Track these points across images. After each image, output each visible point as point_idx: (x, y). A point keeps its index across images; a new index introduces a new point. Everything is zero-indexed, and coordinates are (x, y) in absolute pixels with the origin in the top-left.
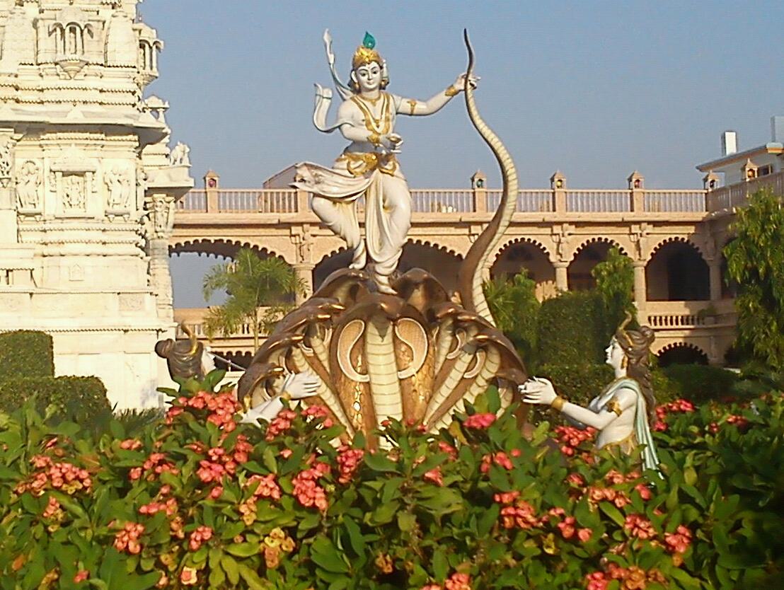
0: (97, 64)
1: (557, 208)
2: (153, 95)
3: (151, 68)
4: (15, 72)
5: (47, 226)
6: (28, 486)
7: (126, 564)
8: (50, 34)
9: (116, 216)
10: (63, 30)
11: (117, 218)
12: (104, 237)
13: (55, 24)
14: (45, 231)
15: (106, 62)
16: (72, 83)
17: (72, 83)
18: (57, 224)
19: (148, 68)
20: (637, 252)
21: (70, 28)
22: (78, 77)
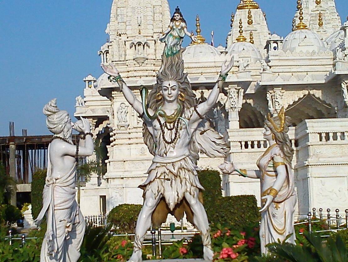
0: (152, 59)
1: (22, 131)
2: (90, 75)
3: (104, 62)
4: (237, 60)
5: (130, 131)
6: (116, 243)
7: (213, 257)
8: (131, 48)
9: (121, 127)
10: (135, 46)
11: (122, 128)
12: (130, 136)
13: (132, 43)
14: (130, 133)
15: (156, 57)
16: (141, 68)
17: (141, 68)
18: (134, 130)
19: (105, 62)
20: (160, 142)
21: (138, 45)
22: (143, 65)
